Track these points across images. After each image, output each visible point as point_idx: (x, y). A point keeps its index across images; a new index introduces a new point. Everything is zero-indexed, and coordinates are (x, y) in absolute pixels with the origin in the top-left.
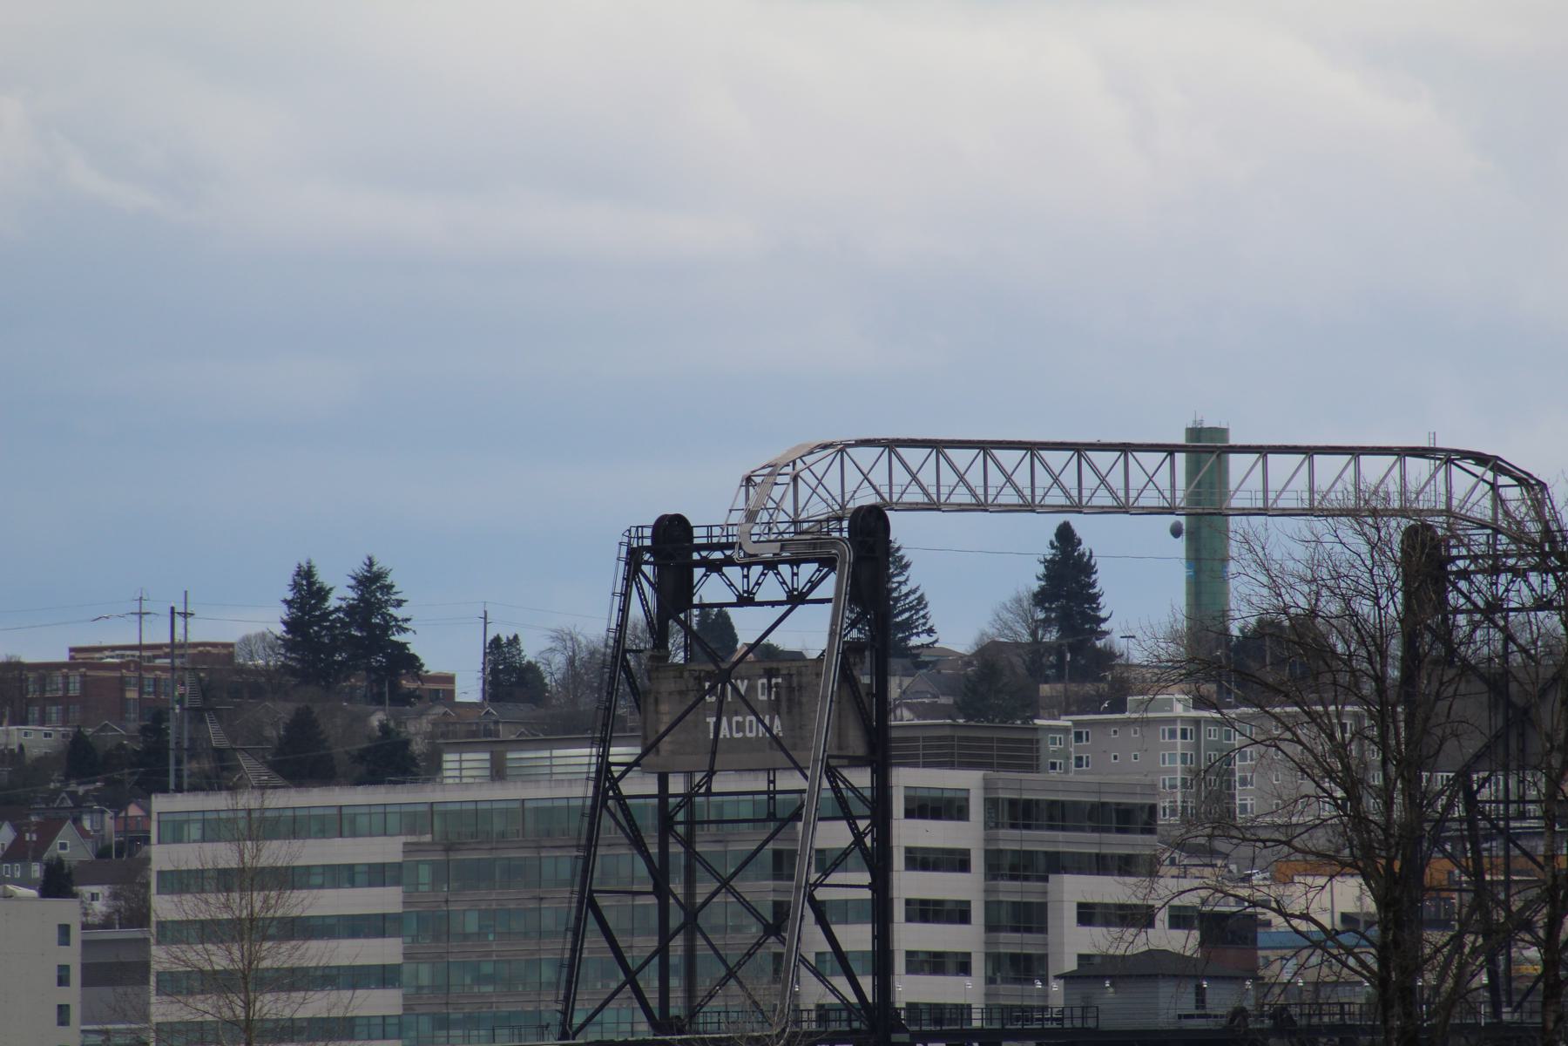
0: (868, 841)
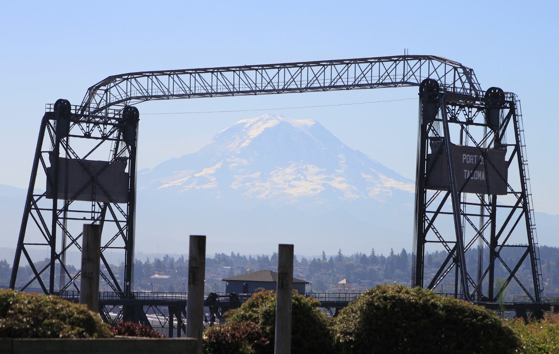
0: (125, 232)
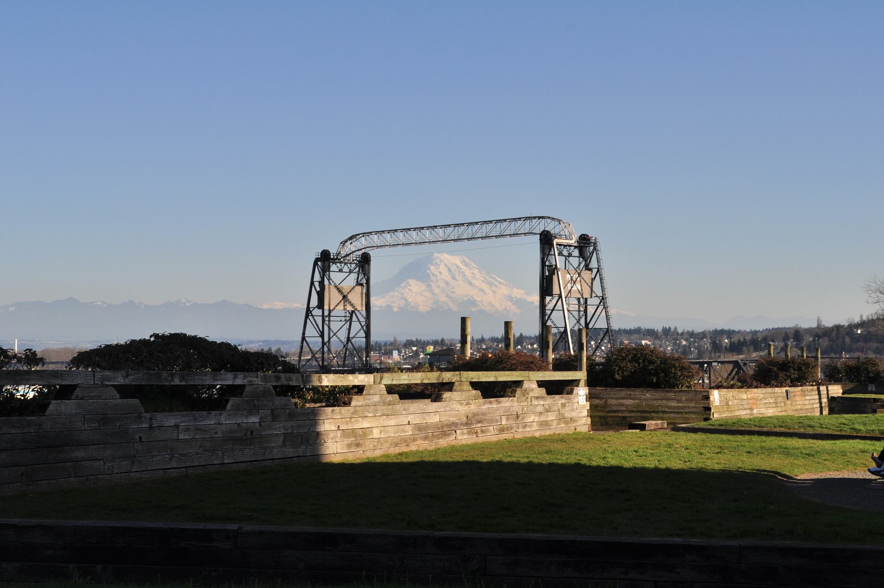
0: (365, 328)
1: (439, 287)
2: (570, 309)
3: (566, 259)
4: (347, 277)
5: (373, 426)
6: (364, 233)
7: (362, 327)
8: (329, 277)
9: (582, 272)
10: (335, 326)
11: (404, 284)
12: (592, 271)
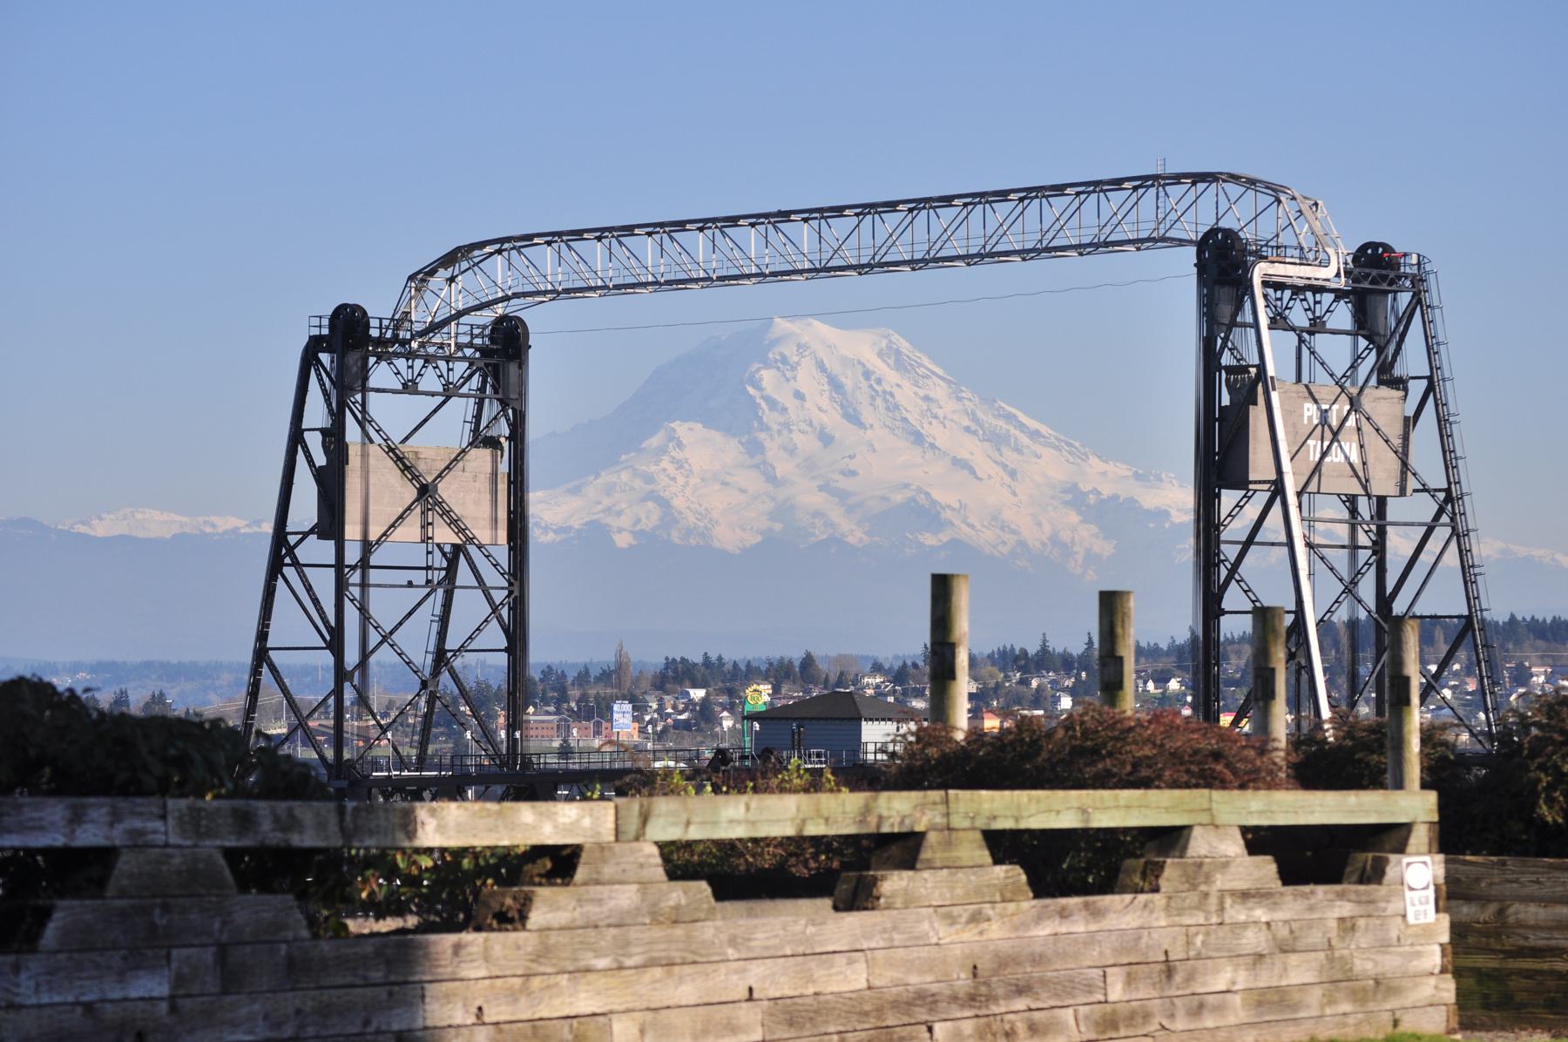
0: (505, 612)
1: (791, 451)
2: (1318, 540)
3: (1301, 341)
4: (435, 411)
5: (615, 1007)
6: (502, 241)
7: (495, 609)
8: (364, 411)
9: (1366, 391)
10: (386, 606)
11: (654, 442)
12: (1406, 390)
